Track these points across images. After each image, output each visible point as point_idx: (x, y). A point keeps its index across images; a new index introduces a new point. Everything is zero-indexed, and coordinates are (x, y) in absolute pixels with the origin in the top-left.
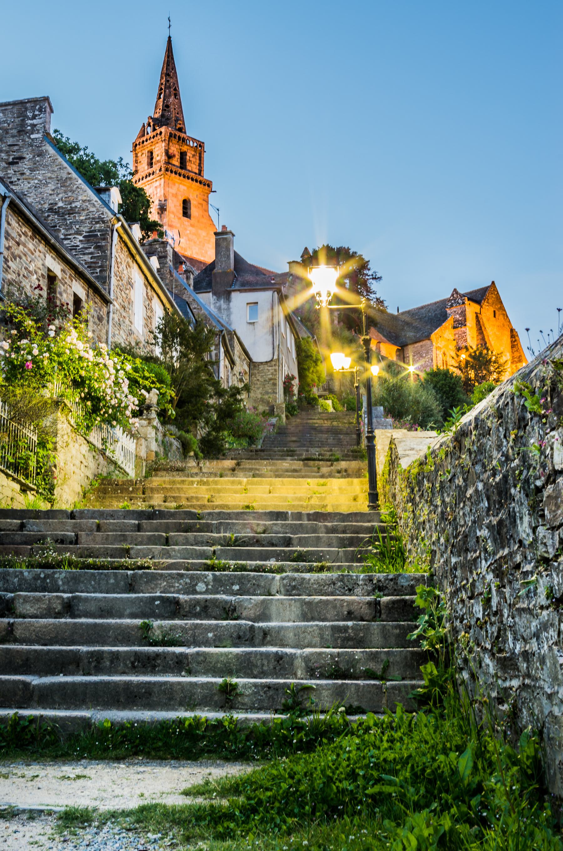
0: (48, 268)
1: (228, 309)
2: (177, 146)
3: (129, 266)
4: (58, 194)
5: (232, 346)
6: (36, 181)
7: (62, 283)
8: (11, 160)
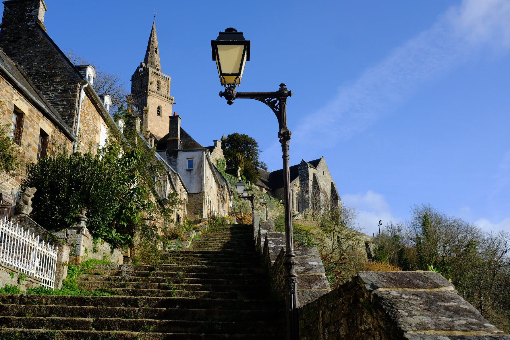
0: (15, 106)
1: (176, 161)
2: (156, 78)
3: (96, 118)
4: (43, 63)
5: (176, 184)
6: (28, 54)
7: (29, 120)
8: (12, 39)
